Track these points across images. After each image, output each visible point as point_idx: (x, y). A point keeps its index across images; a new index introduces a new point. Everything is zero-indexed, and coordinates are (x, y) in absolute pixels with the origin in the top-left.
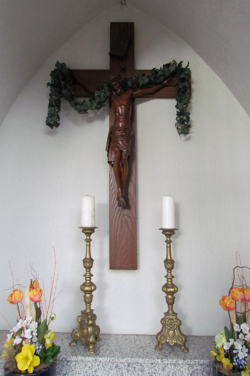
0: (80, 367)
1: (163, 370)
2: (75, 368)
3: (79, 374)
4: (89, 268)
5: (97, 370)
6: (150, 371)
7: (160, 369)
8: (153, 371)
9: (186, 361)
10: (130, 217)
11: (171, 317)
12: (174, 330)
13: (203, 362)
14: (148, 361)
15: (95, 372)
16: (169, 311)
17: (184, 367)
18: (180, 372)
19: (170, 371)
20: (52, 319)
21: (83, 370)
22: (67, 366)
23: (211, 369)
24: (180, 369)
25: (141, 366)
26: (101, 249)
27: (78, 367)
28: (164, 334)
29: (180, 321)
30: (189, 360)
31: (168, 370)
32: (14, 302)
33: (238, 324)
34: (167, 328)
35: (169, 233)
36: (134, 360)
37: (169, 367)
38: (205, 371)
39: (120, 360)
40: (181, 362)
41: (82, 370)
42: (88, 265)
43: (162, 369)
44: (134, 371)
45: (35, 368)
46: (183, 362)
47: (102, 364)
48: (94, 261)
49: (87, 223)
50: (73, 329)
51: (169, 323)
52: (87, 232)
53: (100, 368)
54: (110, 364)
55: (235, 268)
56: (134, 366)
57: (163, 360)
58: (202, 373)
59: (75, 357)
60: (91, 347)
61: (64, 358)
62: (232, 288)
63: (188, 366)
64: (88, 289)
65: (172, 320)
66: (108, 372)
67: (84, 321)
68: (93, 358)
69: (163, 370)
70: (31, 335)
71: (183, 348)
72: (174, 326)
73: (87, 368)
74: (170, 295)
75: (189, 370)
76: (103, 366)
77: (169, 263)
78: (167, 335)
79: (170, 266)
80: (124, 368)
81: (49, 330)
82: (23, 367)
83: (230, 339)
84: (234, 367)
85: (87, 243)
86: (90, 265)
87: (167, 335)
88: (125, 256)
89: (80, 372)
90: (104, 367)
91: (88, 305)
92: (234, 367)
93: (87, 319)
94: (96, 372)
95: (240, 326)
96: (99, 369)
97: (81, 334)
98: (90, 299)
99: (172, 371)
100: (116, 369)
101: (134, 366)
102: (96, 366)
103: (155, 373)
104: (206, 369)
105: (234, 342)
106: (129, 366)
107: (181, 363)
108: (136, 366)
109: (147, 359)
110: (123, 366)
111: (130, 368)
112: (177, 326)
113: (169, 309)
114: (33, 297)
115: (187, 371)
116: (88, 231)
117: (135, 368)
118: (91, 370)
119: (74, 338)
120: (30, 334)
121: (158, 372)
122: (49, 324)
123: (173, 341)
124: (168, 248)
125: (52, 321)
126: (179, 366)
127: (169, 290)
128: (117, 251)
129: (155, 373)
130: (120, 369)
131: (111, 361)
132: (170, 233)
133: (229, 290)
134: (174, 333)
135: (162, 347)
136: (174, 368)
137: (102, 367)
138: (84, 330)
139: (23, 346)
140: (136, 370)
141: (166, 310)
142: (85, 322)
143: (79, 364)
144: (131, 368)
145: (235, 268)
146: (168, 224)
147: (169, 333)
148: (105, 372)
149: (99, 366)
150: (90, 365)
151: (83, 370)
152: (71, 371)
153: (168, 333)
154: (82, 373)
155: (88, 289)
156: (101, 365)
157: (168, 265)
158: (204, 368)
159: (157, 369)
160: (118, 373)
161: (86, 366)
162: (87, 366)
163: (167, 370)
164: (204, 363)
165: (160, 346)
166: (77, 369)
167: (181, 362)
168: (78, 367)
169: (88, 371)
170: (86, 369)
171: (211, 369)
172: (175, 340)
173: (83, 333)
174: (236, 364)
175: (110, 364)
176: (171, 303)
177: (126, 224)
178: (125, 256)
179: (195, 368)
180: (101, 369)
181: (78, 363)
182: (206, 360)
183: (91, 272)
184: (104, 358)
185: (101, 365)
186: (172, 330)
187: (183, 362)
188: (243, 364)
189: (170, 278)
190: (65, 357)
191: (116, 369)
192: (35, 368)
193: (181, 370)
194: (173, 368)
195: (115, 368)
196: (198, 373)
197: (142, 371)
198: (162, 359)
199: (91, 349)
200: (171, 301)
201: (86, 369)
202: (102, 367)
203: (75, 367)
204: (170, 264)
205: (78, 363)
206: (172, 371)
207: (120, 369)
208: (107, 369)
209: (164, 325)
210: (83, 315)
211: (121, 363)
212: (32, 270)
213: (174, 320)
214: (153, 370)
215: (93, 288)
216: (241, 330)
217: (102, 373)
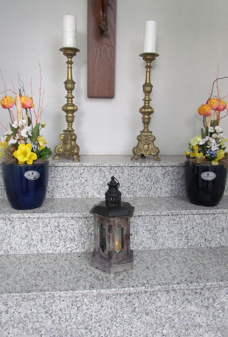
0: (67, 171)
1: (140, 171)
2: (62, 173)
3: (66, 176)
4: (70, 90)
5: (83, 173)
6: (129, 173)
7: (138, 171)
8: (131, 173)
9: (160, 164)
10: (109, 46)
11: (146, 134)
12: (148, 145)
13: (174, 164)
14: (128, 164)
15: (81, 175)
16: (144, 130)
17: (158, 169)
18: (154, 172)
19: (146, 172)
20: (43, 126)
21: (70, 174)
22: (55, 171)
23: (180, 170)
24: (154, 171)
25: (121, 169)
26: (81, 78)
27: (66, 171)
28: (140, 148)
29: (155, 137)
30: (163, 163)
31: (145, 172)
32: (6, 106)
33: (212, 127)
34: (142, 143)
35: (149, 58)
36: (116, 164)
37: (145, 169)
38: (175, 172)
39: (104, 164)
40: (157, 164)
41: (69, 173)
42: (70, 86)
43: (139, 171)
44: (115, 173)
45: (34, 161)
46: (158, 165)
47: (87, 169)
48: (75, 83)
49: (69, 42)
50: (56, 146)
51: (145, 139)
52: (69, 52)
53: (85, 171)
54: (94, 168)
55: (214, 82)
56: (116, 169)
57: (141, 163)
58: (172, 173)
59: (63, 163)
60: (75, 157)
61: (52, 164)
62: (209, 99)
63: (161, 168)
64: (70, 111)
65: (145, 137)
66: (92, 175)
67: (67, 137)
68: (79, 163)
69: (140, 171)
70: (27, 135)
71: (156, 157)
72: (149, 141)
73: (73, 172)
74: (146, 115)
75: (162, 171)
76: (88, 170)
77: (149, 86)
78: (142, 148)
79: (149, 90)
80: (107, 171)
81: (40, 136)
82: (23, 159)
83: (206, 136)
84: (207, 158)
85: (68, 66)
86: (72, 86)
87: (142, 148)
88: (102, 87)
89: (67, 176)
90: (89, 171)
91: (70, 124)
92: (207, 158)
93: (69, 136)
94: (82, 175)
95: (214, 128)
96: (84, 173)
97: (64, 149)
98: (72, 118)
99: (147, 173)
100: (99, 172)
101: (116, 169)
102: (82, 170)
103: (133, 174)
104: (177, 170)
105: (209, 138)
106: (111, 169)
107: (156, 166)
108: (117, 169)
109: (127, 163)
110: (106, 169)
111: (112, 171)
112: (151, 141)
113: (145, 127)
114: (25, 102)
115: (160, 172)
116: (70, 53)
117: (116, 170)
118: (77, 173)
119: (57, 152)
120: (26, 134)
121: (136, 173)
122: (40, 129)
123: (147, 153)
124: (148, 73)
125: (42, 128)
126: (154, 168)
127: (146, 110)
128: (95, 80)
129: (133, 174)
130: (103, 171)
131: (95, 165)
132: (151, 57)
133: (207, 100)
134: (149, 147)
135: (137, 157)
136: (150, 170)
137: (87, 171)
138: (67, 145)
139: (19, 145)
140: (118, 172)
141: (142, 129)
142: (68, 138)
143: (66, 169)
144: (113, 171)
145: (214, 82)
146: (150, 49)
147: (144, 147)
148: (90, 175)
149: (84, 170)
150: (76, 170)
151: (70, 174)
152: (59, 174)
153: (143, 147)
154: (69, 176)
155: (70, 111)
156: (86, 169)
157: (147, 87)
158: (174, 169)
159: (136, 171)
160: (102, 175)
161: (72, 170)
162: (73, 170)
163: (143, 172)
164: (175, 165)
165: (136, 157)
166: (64, 172)
167: (157, 164)
168: (66, 171)
169: (74, 174)
170: (72, 173)
171: (180, 170)
172: (149, 152)
173: (66, 148)
174: (209, 155)
175: (94, 168)
176: (146, 123)
177: (105, 53)
178: (102, 87)
179: (167, 169)
180: (86, 173)
181: (65, 169)
182: (177, 163)
183: (73, 94)
184: (89, 163)
185: (86, 169)
186: (147, 144)
187: (158, 165)
188: (215, 154)
189: (147, 101)
190: (53, 163)
191: (99, 172)
192: (34, 161)
193: (155, 171)
194: (149, 170)
195: (99, 171)
196: (170, 173)
197: (122, 173)
198: (140, 163)
199: (75, 158)
200: (147, 120)
201: (72, 173)
202: (87, 171)
203: (62, 172)
204: (148, 88)
205: (65, 169)
206: (147, 173)
207: (103, 171)
208: (91, 172)
209: (139, 140)
210: (66, 133)
211: (104, 167)
212: (20, 81)
213: (150, 136)
214: (132, 172)
215: (75, 108)
216: (216, 130)
217: (87, 175)
